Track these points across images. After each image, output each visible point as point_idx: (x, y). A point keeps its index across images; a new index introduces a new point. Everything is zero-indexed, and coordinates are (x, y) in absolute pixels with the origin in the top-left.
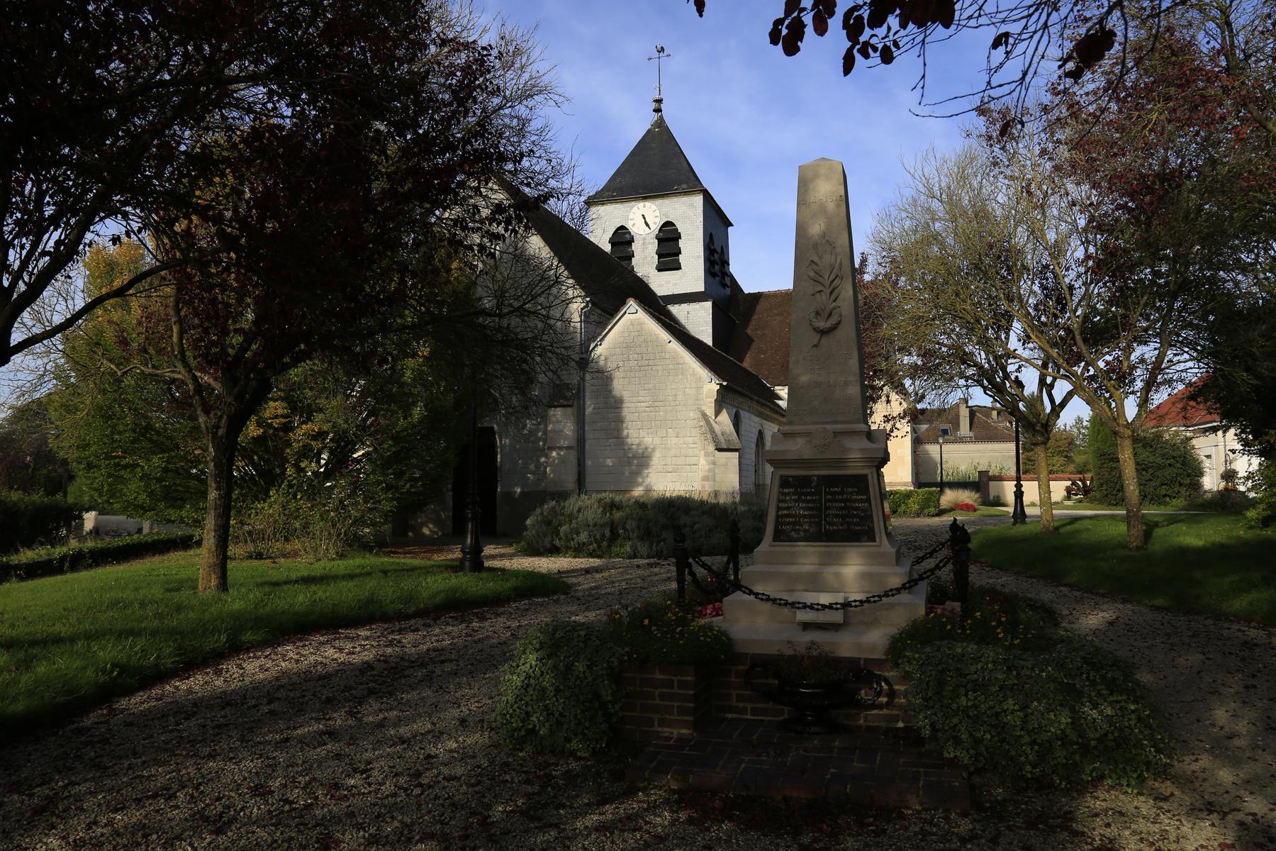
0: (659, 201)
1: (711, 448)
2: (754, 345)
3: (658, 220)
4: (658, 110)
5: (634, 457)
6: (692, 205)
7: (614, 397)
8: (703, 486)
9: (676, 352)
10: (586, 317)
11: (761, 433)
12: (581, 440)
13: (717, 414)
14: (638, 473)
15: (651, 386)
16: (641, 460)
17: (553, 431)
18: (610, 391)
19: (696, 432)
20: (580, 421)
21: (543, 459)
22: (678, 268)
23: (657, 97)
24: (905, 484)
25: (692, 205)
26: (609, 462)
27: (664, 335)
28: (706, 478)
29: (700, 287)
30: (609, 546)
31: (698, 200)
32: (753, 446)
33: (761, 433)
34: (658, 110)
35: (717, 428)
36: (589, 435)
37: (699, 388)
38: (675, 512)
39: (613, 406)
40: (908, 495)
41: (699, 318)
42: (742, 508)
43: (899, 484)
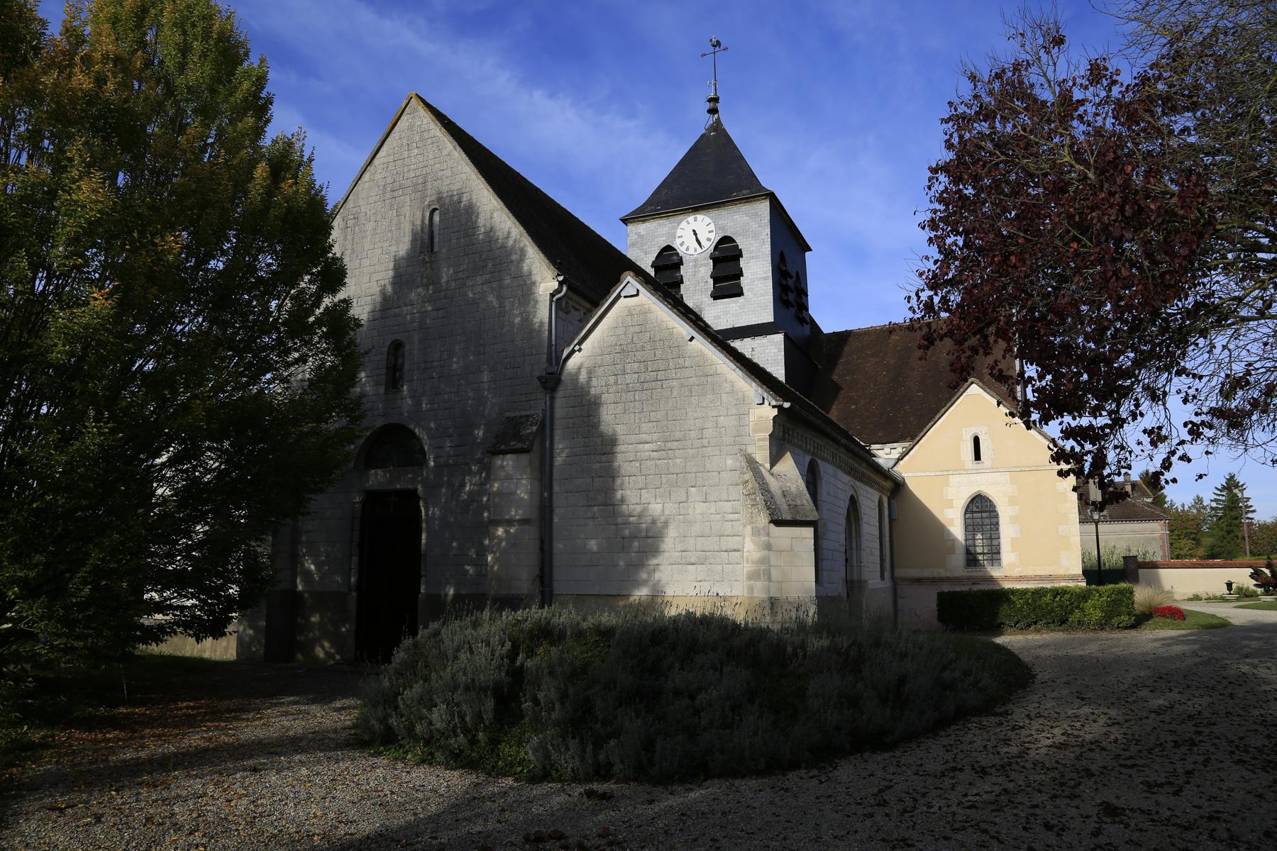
0: (715, 212)
1: (763, 519)
2: (842, 394)
3: (712, 236)
4: (713, 111)
5: (633, 537)
6: (756, 215)
7: (601, 435)
8: (751, 589)
9: (702, 355)
10: (560, 304)
11: (853, 501)
12: (545, 509)
13: (774, 460)
14: (639, 564)
15: (660, 415)
16: (641, 543)
17: (500, 493)
18: (596, 426)
19: (737, 493)
20: (544, 476)
21: (487, 542)
22: (740, 293)
23: (712, 95)
24: (1073, 578)
25: (756, 215)
26: (593, 545)
27: (683, 329)
28: (753, 576)
29: (768, 316)
30: (494, 742)
31: (764, 207)
32: (843, 521)
33: (853, 501)
34: (713, 111)
35: (774, 485)
36: (559, 500)
37: (742, 416)
38: (707, 637)
39: (600, 449)
40: (1084, 596)
41: (770, 353)
42: (817, 643)
43: (1064, 578)
